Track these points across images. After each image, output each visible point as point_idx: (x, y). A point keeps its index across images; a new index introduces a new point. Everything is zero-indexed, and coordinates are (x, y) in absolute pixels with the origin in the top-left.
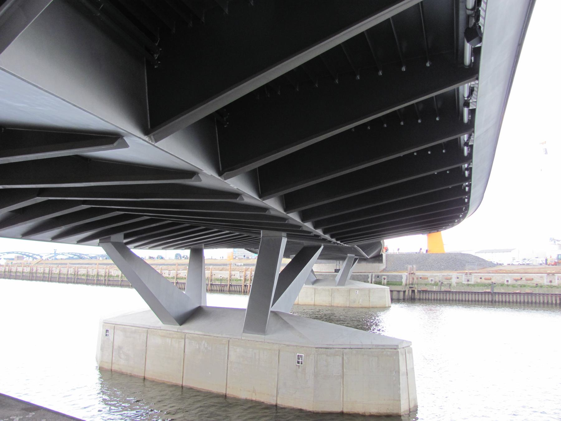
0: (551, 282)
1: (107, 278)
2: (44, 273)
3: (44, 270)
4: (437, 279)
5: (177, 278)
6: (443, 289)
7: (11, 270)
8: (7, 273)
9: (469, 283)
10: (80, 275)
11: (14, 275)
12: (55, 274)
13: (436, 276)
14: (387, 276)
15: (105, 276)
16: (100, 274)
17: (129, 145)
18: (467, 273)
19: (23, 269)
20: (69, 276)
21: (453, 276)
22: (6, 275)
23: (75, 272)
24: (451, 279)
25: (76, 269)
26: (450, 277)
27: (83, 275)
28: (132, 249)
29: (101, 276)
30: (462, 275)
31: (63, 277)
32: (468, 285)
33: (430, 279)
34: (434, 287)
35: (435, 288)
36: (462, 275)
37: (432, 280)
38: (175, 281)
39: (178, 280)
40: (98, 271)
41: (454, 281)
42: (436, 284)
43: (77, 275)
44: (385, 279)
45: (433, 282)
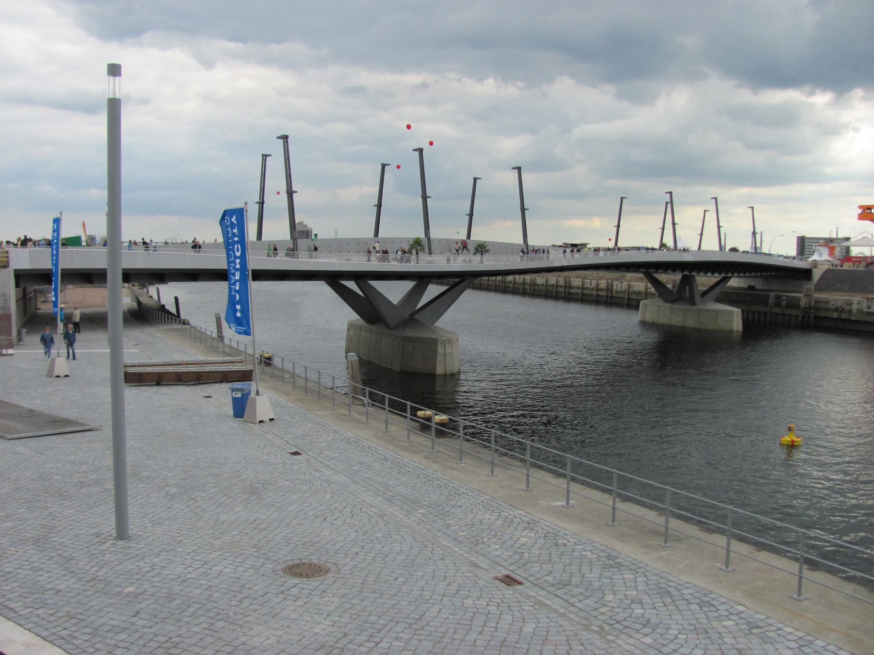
0: (869, 308)
1: (567, 289)
2: (557, 286)
3: (598, 285)
4: (839, 304)
5: (629, 293)
6: (844, 316)
7: (570, 284)
8: (527, 287)
9: (870, 310)
10: (508, 282)
11: (603, 296)
12: (588, 288)
13: (838, 300)
14: (787, 297)
15: (531, 284)
16: (526, 281)
17: (122, 314)
18: (869, 298)
19: (515, 279)
20: (497, 284)
21: (854, 301)
22: (526, 289)
23: (566, 283)
24: (852, 304)
25: (568, 279)
26: (851, 302)
27: (511, 282)
28: (853, 246)
29: (527, 284)
30: (863, 301)
31: (636, 298)
32: (868, 313)
33: (831, 303)
34: (835, 313)
35: (835, 315)
36: (863, 301)
37: (833, 305)
38: (594, 293)
39: (598, 292)
40: (629, 284)
41: (855, 307)
42: (836, 310)
43: (505, 282)
44: (784, 300)
45: (834, 307)
